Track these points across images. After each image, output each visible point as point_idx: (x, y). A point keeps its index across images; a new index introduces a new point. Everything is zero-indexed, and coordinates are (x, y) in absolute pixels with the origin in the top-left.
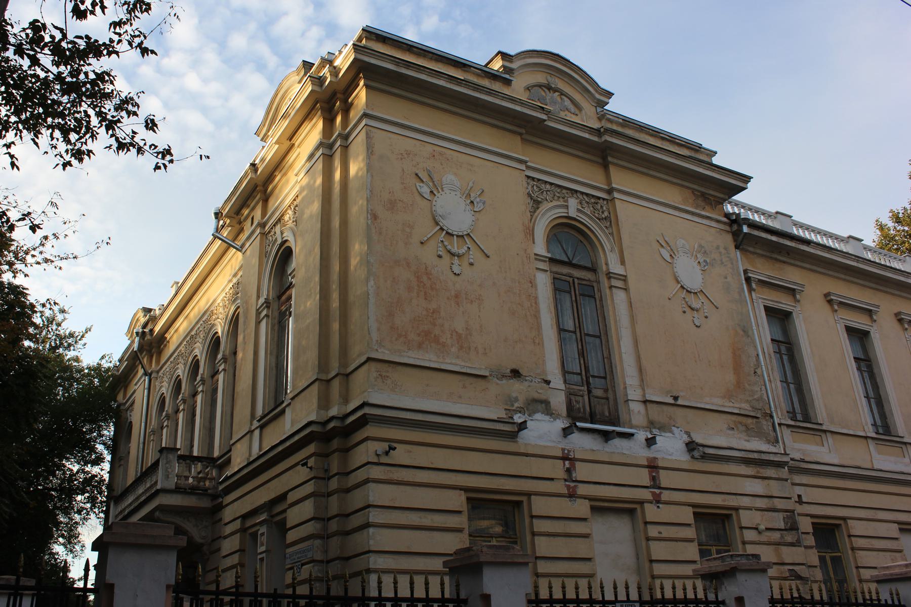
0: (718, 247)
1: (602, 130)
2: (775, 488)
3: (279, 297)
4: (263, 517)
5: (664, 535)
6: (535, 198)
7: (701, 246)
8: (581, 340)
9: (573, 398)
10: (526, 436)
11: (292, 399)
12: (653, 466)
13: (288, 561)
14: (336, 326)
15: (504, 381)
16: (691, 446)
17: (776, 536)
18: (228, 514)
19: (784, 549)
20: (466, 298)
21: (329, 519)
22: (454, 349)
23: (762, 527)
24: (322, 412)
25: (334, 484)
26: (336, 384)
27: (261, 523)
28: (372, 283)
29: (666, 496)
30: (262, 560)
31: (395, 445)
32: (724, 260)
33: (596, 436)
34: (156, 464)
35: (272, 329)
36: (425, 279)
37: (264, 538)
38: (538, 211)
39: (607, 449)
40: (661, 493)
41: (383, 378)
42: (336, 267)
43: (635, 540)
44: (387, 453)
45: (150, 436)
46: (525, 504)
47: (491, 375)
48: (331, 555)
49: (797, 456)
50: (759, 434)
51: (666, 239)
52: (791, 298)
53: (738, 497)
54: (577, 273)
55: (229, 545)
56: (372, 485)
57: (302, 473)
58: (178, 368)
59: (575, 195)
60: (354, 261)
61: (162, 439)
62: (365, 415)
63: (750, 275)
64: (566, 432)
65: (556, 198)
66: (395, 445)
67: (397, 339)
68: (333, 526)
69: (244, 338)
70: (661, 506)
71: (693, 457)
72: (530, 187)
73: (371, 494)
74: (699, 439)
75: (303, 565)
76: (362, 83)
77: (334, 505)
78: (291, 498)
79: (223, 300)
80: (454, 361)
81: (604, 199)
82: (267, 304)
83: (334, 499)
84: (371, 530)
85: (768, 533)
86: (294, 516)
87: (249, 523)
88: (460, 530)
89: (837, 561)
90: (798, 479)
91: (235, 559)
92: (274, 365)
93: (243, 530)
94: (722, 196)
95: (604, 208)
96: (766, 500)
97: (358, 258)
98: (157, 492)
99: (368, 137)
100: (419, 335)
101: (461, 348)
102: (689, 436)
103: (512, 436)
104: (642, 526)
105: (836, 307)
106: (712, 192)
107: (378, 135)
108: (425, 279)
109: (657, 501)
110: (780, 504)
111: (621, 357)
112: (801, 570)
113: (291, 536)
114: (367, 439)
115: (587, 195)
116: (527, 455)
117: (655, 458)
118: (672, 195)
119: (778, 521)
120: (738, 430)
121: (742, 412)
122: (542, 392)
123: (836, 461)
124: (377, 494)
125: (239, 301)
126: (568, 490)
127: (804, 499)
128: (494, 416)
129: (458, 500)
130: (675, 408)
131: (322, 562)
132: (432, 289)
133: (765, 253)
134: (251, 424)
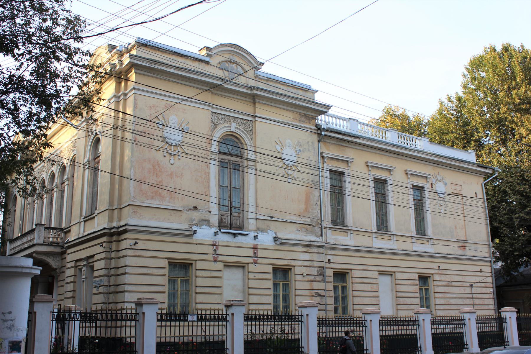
0: (308, 142)
1: (253, 88)
2: (315, 257)
3: (95, 159)
4: (84, 263)
5: (257, 277)
6: (215, 123)
7: (299, 142)
8: (230, 190)
9: (223, 217)
10: (198, 237)
11: (98, 214)
12: (255, 248)
13: (94, 284)
14: (117, 186)
15: (190, 212)
16: (276, 239)
17: (312, 278)
18: (69, 258)
19: (315, 283)
20: (175, 175)
21: (111, 269)
22: (168, 199)
23: (305, 274)
24: (110, 223)
25: (113, 255)
26: (116, 212)
27: (83, 265)
28: (132, 170)
29: (260, 261)
30: (83, 281)
31: (138, 241)
32: (310, 149)
33: (230, 235)
34: (33, 230)
35: (91, 175)
36: (157, 167)
37: (85, 272)
38: (216, 130)
39: (234, 241)
40: (257, 260)
41: (135, 212)
42: (118, 159)
43: (244, 279)
44: (135, 244)
45: (27, 206)
46: (194, 265)
47: (183, 210)
48: (111, 284)
49: (332, 242)
50: (313, 233)
51: (280, 140)
52: (346, 164)
53: (295, 261)
54: (232, 158)
55: (69, 272)
56: (127, 258)
57: (99, 249)
58: (42, 174)
59: (236, 120)
60: (126, 158)
61: (34, 208)
62: (126, 229)
63: (324, 155)
64: (216, 233)
65: (226, 122)
66: (138, 241)
67: (142, 196)
68: (112, 272)
69: (77, 175)
70: (257, 265)
71: (276, 244)
72: (213, 118)
73: (127, 261)
74: (280, 235)
75: (100, 286)
76: (133, 71)
77: (113, 264)
78: (96, 257)
79: (67, 147)
80: (167, 204)
81: (251, 121)
82: (89, 162)
83: (113, 261)
84: (126, 275)
85: (308, 277)
86: (97, 266)
87: (78, 264)
88: (164, 275)
89: (344, 288)
90: (330, 252)
91: (71, 279)
92: (91, 192)
93: (76, 267)
94: (315, 115)
95: (251, 125)
96: (310, 262)
97: (127, 158)
98: (34, 245)
99: (135, 99)
100: (152, 193)
101: (171, 198)
102: (276, 234)
103: (191, 236)
104: (247, 273)
105: (370, 169)
106: (310, 113)
107: (140, 98)
108: (157, 167)
109: (255, 263)
110: (316, 264)
111: (248, 198)
112: (322, 293)
113: (96, 274)
114: (126, 239)
115: (242, 119)
116: (197, 244)
117: (257, 245)
118: (287, 116)
119: (314, 271)
120: (302, 231)
121: (305, 223)
122: (207, 216)
123: (352, 244)
124: (129, 261)
125: (75, 152)
126: (214, 258)
127: (331, 261)
128: (183, 228)
129: (164, 263)
130: (271, 221)
131: (107, 286)
132: (160, 171)
133: (335, 143)
134: (80, 219)
